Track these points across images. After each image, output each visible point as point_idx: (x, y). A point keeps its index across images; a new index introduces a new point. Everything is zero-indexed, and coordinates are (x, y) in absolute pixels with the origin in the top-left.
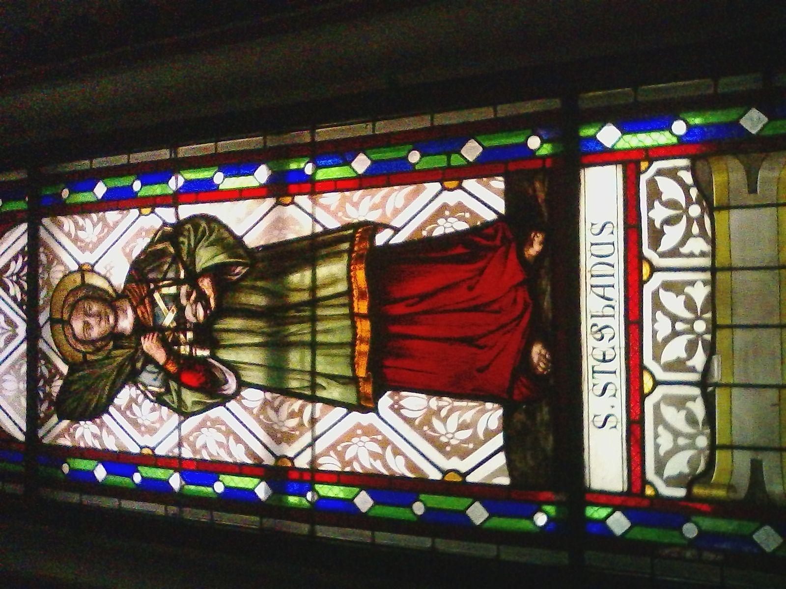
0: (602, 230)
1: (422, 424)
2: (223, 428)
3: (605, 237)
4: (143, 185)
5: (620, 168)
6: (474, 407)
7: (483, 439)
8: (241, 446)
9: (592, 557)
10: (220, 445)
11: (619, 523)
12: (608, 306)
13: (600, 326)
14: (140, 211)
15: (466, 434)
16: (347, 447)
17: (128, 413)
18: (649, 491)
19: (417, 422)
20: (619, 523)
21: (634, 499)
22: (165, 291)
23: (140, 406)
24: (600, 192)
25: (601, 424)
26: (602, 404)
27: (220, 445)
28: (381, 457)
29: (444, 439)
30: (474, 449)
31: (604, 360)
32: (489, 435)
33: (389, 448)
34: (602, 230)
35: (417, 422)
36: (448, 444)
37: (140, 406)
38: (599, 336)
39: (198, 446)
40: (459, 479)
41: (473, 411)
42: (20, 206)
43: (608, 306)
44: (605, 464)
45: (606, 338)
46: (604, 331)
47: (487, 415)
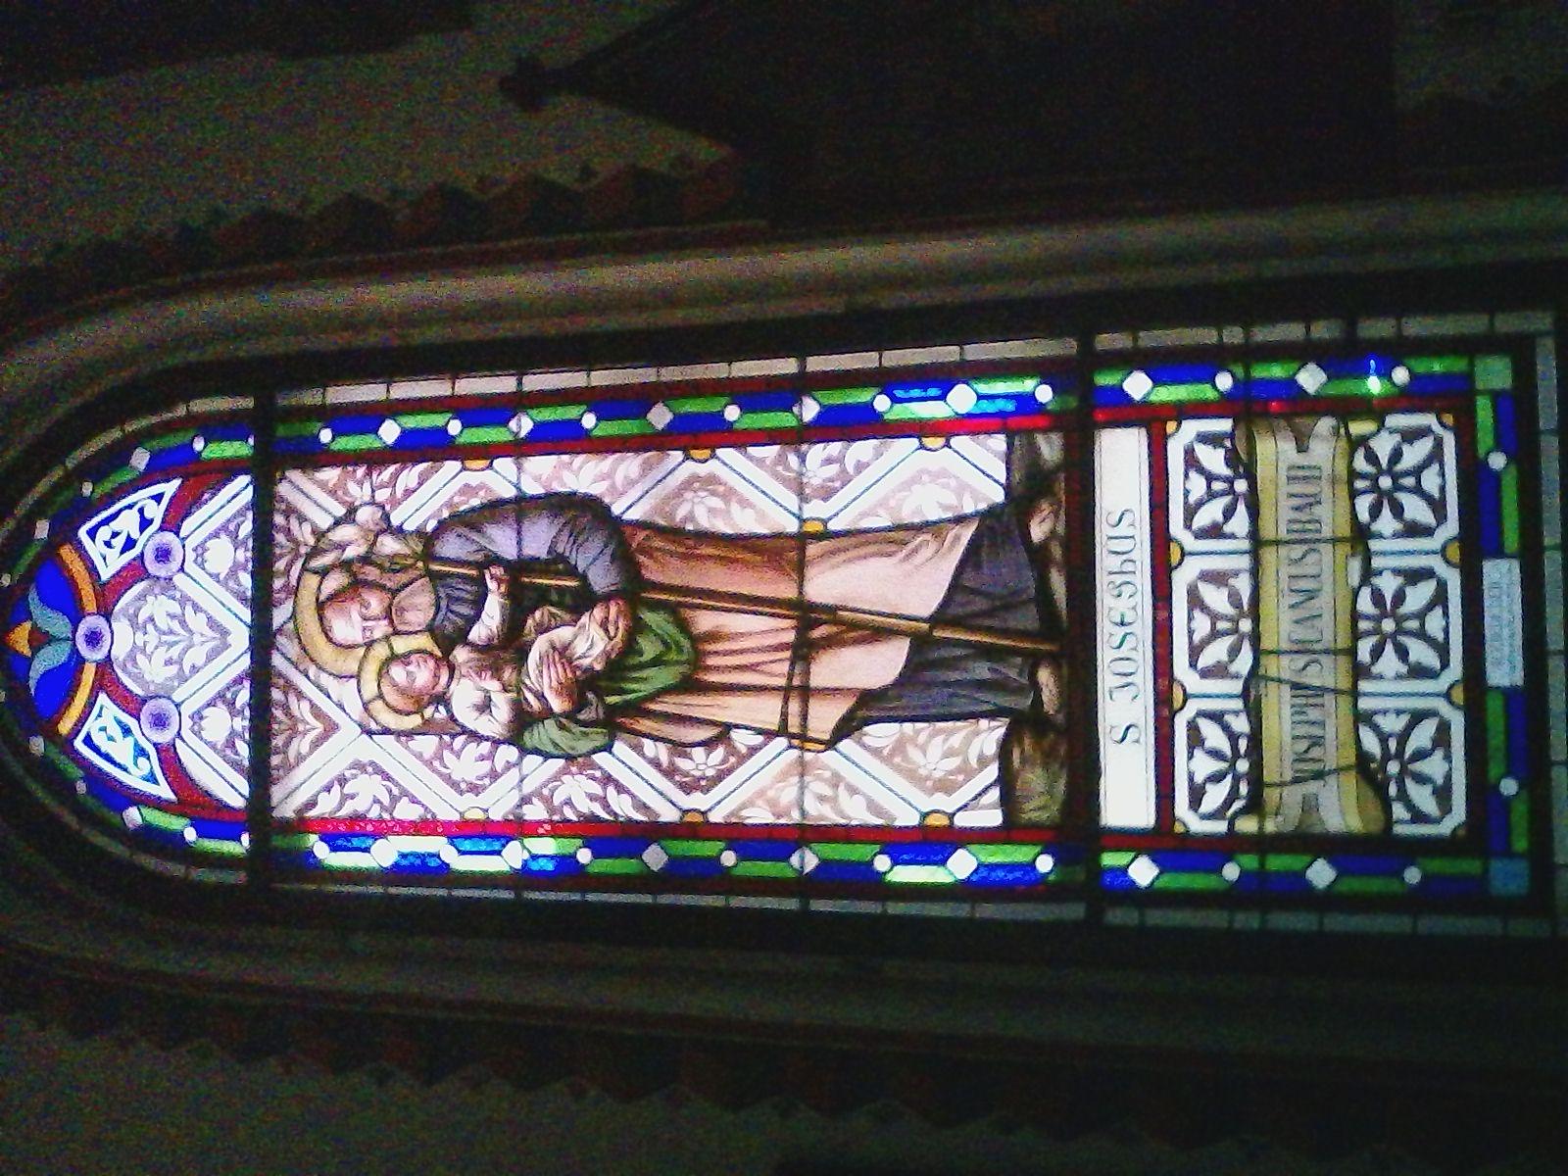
0: (1120, 520)
1: (892, 755)
2: (598, 774)
3: (1123, 530)
4: (464, 426)
5: (1143, 431)
6: (964, 727)
7: (976, 766)
8: (625, 796)
9: (1117, 916)
10: (592, 798)
11: (1143, 872)
12: (1131, 674)
13: (1118, 583)
14: (952, 822)
15: (954, 763)
16: (724, 761)
17: (436, 764)
18: (1179, 828)
19: (885, 752)
20: (1143, 872)
21: (1162, 840)
22: (493, 571)
23: (149, 658)
24: (1120, 456)
25: (1118, 643)
26: (1123, 708)
27: (592, 798)
28: (833, 801)
29: (923, 772)
30: (966, 781)
31: (1122, 624)
32: (983, 761)
33: (842, 787)
34: (1120, 520)
35: (885, 752)
36: (927, 778)
37: (149, 658)
38: (1116, 592)
39: (556, 802)
40: (945, 821)
41: (963, 734)
42: (238, 449)
43: (1131, 674)
44: (1125, 798)
45: (1125, 595)
46: (1123, 588)
47: (982, 736)
